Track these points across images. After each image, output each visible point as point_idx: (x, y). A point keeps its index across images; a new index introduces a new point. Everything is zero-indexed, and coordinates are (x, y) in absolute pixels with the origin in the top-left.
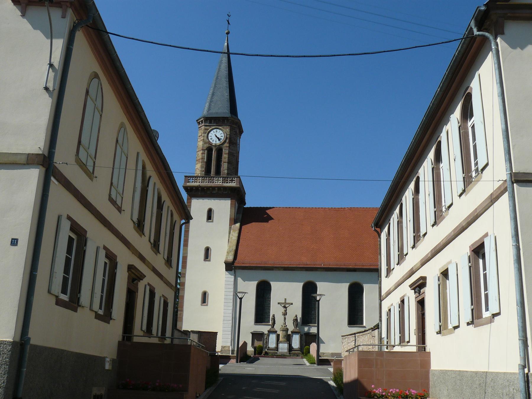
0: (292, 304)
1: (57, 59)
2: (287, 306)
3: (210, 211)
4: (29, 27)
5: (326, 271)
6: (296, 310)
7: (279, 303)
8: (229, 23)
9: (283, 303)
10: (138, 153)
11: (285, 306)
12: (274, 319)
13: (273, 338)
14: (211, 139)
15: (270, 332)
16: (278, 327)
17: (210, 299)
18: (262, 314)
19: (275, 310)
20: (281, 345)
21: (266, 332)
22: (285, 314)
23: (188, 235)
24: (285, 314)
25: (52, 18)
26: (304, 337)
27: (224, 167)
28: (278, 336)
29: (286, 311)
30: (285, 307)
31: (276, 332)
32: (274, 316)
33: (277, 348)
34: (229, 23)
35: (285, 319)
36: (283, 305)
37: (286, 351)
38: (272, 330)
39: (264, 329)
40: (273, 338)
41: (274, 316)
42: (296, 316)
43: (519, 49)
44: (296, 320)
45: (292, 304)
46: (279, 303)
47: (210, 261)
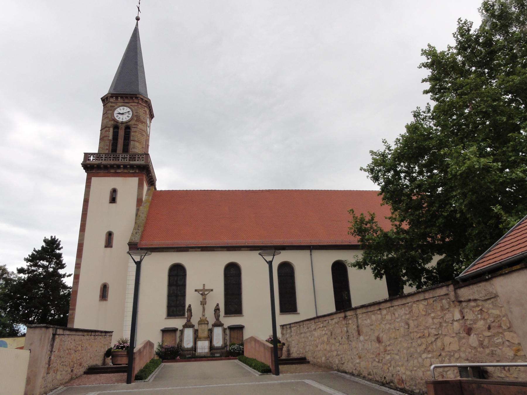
0: (212, 290)
2: (206, 293)
3: (114, 191)
4: (157, 182)
5: (250, 250)
6: (218, 297)
7: (196, 291)
8: (139, 10)
9: (201, 290)
10: (107, 333)
12: (190, 310)
13: (189, 334)
14: (128, 117)
15: (186, 326)
16: (195, 321)
17: (111, 293)
18: (176, 305)
19: (191, 298)
20: (200, 344)
21: (180, 328)
22: (203, 303)
23: (86, 218)
24: (203, 303)
25: (156, 243)
26: (228, 332)
27: (121, 133)
28: (196, 332)
29: (205, 299)
31: (192, 326)
32: (190, 306)
33: (195, 348)
34: (139, 10)
36: (201, 292)
37: (207, 350)
39: (177, 323)
41: (190, 306)
42: (218, 305)
43: (446, 42)
44: (217, 310)
45: (212, 290)
46: (196, 291)
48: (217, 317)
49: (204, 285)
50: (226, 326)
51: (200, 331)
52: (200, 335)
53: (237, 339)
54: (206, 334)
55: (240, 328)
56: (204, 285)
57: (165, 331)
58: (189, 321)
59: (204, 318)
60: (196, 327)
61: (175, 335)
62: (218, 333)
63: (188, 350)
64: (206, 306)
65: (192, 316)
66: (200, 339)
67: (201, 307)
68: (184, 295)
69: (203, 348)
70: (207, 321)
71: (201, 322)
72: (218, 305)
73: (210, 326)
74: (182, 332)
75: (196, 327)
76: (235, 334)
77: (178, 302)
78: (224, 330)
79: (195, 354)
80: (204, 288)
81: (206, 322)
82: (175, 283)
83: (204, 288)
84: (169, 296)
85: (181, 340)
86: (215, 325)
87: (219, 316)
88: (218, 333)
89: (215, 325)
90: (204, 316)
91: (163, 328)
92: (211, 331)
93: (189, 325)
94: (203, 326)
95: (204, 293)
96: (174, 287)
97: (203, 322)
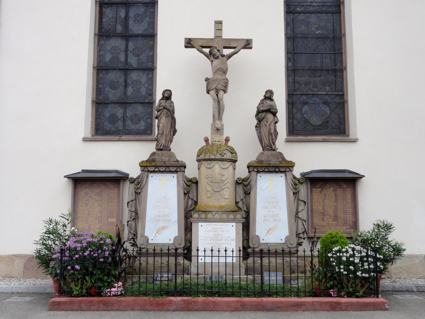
0: (248, 44)
1: (311, 246)
6: (265, 68)
11: (217, 50)
13: (163, 195)
15: (150, 166)
16: (185, 147)
19: (175, 70)
21: (134, 172)
22: (217, 87)
24: (217, 87)
28: (190, 187)
30: (212, 56)
31: (178, 168)
33: (186, 249)
35: (219, 110)
38: (163, 157)
39: (124, 156)
40: (163, 195)
42: (269, 96)
44: (265, 111)
45: (248, 44)
47: (186, 39)
48: (268, 142)
49: (219, 23)
50: (297, 172)
51: (204, 187)
52: (206, 198)
53: (336, 218)
54: (227, 197)
55: (348, 182)
56: (219, 23)
57: (80, 182)
58: (164, 148)
59: (220, 139)
60: (191, 172)
61: (120, 197)
62: (272, 199)
63: (158, 252)
64: (227, 99)
65: (175, 131)
66: (207, 215)
67: (209, 101)
68: (149, 69)
69: (279, 260)
70: (232, 151)
71: (209, 154)
72: (269, 96)
73: (242, 171)
74: (139, 185)
75: (191, 172)
76: (327, 200)
77: (130, 90)
78: (295, 184)
79: (186, 271)
80: (218, 37)
81: (228, 156)
82: (119, 28)
83: (218, 37)
84: (101, 69)
85: (137, 216)
86: (259, 167)
87: (274, 135)
88: (272, 199)
89: (259, 167)
90: (218, 130)
91: (76, 168)
92: (245, 186)
93: (161, 163)
94: (217, 167)
95: (217, 50)
96: (117, 43)
97: (215, 152)
